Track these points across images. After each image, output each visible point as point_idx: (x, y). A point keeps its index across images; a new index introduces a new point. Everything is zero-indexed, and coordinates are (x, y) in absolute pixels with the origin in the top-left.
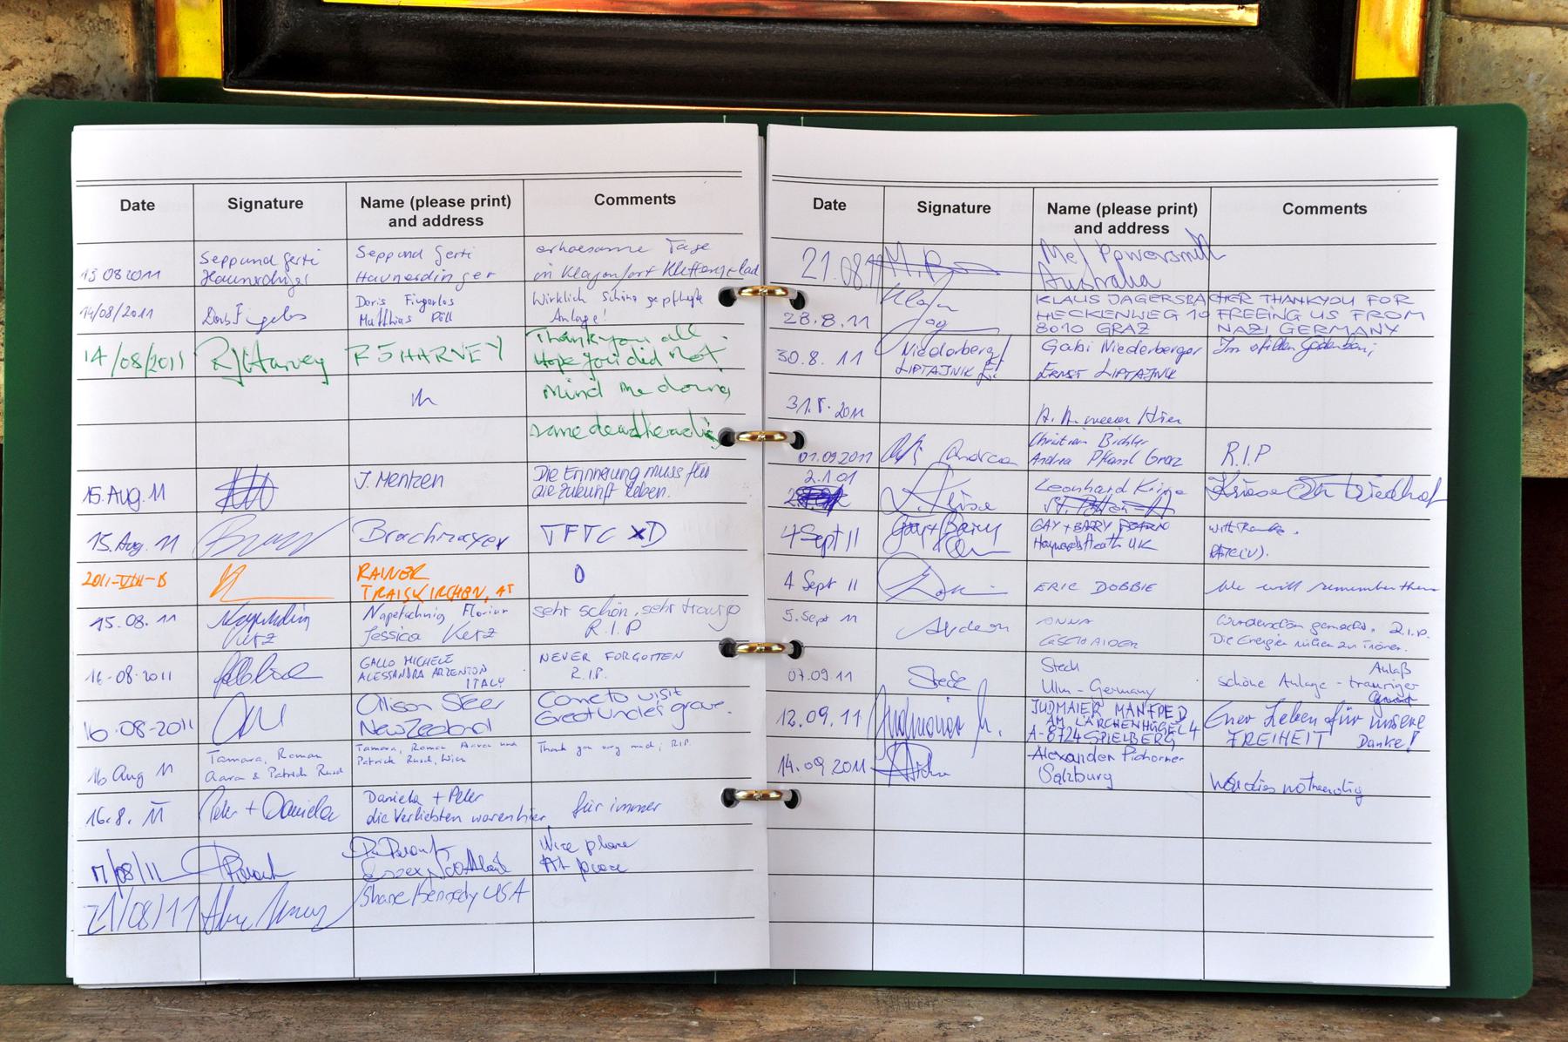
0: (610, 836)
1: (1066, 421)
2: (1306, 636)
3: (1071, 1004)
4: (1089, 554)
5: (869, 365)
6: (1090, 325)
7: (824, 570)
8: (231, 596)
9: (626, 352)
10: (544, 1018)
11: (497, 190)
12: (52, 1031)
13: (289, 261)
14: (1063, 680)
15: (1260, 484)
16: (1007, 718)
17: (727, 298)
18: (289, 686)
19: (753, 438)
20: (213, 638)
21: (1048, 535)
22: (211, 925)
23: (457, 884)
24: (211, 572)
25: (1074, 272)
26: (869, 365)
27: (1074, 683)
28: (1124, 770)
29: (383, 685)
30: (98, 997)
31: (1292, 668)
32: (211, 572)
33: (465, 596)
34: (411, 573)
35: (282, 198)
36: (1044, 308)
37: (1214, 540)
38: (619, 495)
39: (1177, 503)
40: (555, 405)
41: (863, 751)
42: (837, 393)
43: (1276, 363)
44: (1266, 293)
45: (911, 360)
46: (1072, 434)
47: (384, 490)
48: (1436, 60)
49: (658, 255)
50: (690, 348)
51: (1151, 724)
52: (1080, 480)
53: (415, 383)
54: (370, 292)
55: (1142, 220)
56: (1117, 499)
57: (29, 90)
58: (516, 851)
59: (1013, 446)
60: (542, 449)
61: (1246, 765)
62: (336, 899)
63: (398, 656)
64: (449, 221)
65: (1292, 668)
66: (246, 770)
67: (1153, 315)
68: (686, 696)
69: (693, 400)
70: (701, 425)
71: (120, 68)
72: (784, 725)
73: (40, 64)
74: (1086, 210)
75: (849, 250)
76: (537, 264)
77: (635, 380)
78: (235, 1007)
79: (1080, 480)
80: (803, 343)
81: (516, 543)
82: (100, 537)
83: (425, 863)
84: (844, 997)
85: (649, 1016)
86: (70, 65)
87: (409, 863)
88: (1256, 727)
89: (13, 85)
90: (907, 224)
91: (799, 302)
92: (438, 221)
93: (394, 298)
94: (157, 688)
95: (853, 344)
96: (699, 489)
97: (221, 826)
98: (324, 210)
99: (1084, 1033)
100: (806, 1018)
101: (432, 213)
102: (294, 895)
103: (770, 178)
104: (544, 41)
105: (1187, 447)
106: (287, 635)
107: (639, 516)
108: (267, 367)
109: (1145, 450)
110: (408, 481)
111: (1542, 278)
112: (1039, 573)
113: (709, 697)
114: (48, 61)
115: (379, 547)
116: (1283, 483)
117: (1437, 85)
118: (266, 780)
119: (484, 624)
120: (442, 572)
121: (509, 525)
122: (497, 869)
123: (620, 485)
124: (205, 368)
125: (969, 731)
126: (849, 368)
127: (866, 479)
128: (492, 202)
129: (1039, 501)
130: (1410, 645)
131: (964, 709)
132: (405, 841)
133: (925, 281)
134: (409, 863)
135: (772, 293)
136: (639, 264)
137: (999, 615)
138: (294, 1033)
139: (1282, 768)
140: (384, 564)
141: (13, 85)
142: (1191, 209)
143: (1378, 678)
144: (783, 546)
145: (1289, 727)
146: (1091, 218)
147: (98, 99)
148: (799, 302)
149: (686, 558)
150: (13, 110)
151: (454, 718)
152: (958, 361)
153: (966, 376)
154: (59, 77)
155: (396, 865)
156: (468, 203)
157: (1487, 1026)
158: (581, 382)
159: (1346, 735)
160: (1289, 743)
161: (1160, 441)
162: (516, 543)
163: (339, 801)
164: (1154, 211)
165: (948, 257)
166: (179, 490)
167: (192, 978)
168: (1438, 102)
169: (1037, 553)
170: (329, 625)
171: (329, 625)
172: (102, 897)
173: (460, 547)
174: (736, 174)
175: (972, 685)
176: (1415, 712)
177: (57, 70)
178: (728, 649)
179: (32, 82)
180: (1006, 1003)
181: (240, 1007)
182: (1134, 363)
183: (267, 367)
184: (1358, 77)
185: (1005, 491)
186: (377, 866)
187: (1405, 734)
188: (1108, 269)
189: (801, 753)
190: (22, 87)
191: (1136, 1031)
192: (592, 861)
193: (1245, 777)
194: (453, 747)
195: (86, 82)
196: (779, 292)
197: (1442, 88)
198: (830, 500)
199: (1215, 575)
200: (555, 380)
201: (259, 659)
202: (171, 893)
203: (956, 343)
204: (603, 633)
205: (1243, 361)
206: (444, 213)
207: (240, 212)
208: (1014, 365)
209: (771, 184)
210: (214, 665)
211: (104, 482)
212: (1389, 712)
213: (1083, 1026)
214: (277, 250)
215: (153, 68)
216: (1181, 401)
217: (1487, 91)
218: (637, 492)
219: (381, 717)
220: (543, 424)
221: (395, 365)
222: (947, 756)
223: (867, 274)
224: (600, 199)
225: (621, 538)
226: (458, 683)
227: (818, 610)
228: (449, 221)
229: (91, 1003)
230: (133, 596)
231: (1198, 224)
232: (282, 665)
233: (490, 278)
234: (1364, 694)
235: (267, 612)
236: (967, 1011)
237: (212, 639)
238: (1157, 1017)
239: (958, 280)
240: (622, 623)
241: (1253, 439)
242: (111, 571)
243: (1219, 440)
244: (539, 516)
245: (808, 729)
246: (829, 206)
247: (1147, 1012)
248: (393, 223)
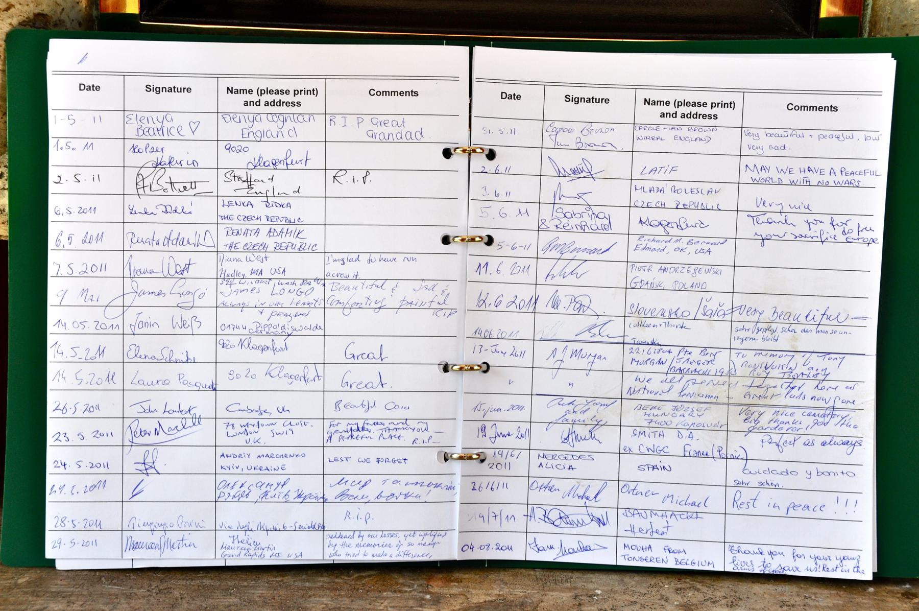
3: (653, 581)
10: (337, 593)
12: (39, 603)
19: (463, 240)
30: (68, 577)
35: (178, 86)
48: (870, 6)
55: (701, 110)
57: (20, 24)
71: (77, 9)
73: (26, 8)
74: (668, 103)
78: (150, 586)
84: (516, 576)
85: (400, 592)
86: (45, 8)
89: (9, 21)
90: (559, 109)
91: (491, 155)
92: (274, 103)
98: (204, 95)
99: (663, 602)
100: (496, 592)
103: (474, 80)
114: (31, 5)
117: (870, 22)
128: (307, 92)
135: (474, 151)
138: (186, 605)
141: (9, 21)
146: (671, 109)
147: (63, 29)
148: (491, 155)
150: (11, 37)
154: (38, 16)
156: (292, 93)
157: (903, 595)
164: (709, 106)
168: (870, 33)
174: (455, 79)
177: (37, 11)
179: (21, 19)
180: (615, 578)
181: (154, 585)
190: (15, 22)
191: (694, 601)
195: (55, 18)
196: (479, 150)
197: (874, 24)
207: (152, 94)
209: (474, 84)
213: (662, 597)
215: (97, 9)
217: (904, 26)
224: (372, 92)
229: (64, 583)
236: (591, 586)
238: (705, 589)
246: (510, 97)
247: (699, 586)
248: (246, 104)
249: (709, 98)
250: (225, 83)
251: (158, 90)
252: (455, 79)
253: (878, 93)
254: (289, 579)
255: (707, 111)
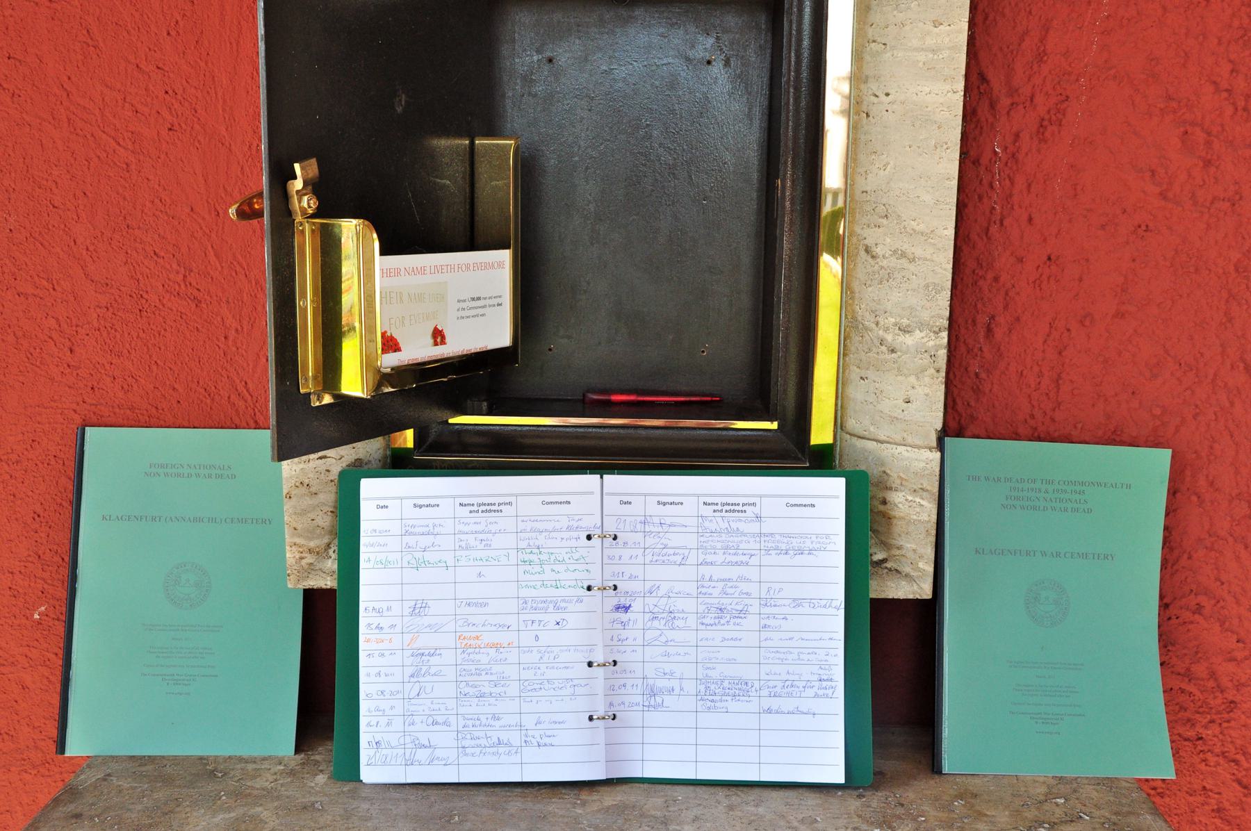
0: (548, 733)
1: (710, 580)
2: (796, 656)
3: (712, 790)
4: (719, 627)
5: (640, 560)
6: (719, 545)
7: (624, 634)
8: (415, 646)
9: (553, 558)
11: (507, 500)
13: (434, 526)
14: (710, 673)
15: (780, 602)
16: (690, 687)
17: (589, 537)
18: (435, 678)
20: (408, 661)
21: (705, 621)
22: (409, 763)
23: (494, 750)
24: (407, 637)
25: (713, 526)
26: (640, 560)
27: (714, 674)
28: (732, 705)
29: (467, 678)
31: (791, 669)
32: (407, 637)
33: (497, 647)
34: (477, 638)
36: (702, 539)
37: (763, 622)
38: (551, 609)
39: (751, 610)
40: (528, 577)
41: (639, 699)
42: (629, 570)
43: (784, 559)
44: (781, 534)
45: (655, 558)
46: (713, 584)
47: (468, 608)
49: (564, 522)
50: (576, 556)
51: (741, 688)
52: (716, 601)
53: (478, 570)
54: (463, 537)
55: (736, 508)
56: (729, 608)
58: (515, 738)
59: (692, 588)
60: (524, 593)
61: (775, 703)
62: (452, 754)
63: (473, 667)
64: (490, 511)
65: (791, 669)
66: (421, 708)
67: (741, 542)
68: (576, 682)
69: (577, 575)
70: (580, 584)
72: (611, 690)
75: (633, 519)
76: (521, 526)
77: (554, 567)
79: (716, 601)
80: (616, 552)
81: (514, 627)
82: (369, 625)
83: (483, 742)
86: (361, 456)
87: (478, 742)
88: (778, 689)
92: (487, 511)
93: (471, 539)
94: (389, 679)
95: (634, 552)
96: (580, 607)
97: (412, 728)
98: (447, 507)
101: (484, 508)
102: (438, 753)
104: (538, 436)
105: (753, 588)
106: (434, 660)
107: (558, 617)
108: (427, 564)
109: (739, 590)
110: (476, 605)
111: (875, 527)
112: (701, 635)
113: (583, 682)
115: (466, 629)
116: (787, 602)
118: (427, 712)
119: (500, 656)
120: (487, 638)
121: (512, 620)
122: (509, 744)
123: (551, 606)
124: (405, 564)
125: (677, 691)
126: (633, 561)
127: (640, 600)
129: (701, 608)
130: (832, 660)
131: (675, 684)
132: (476, 734)
133: (660, 529)
134: (478, 742)
136: (558, 526)
137: (687, 650)
139: (787, 704)
140: (468, 635)
142: (754, 504)
143: (821, 672)
144: (610, 626)
145: (790, 689)
146: (719, 507)
148: (615, 538)
149: (575, 632)
151: (493, 690)
152: (672, 558)
153: (675, 564)
155: (473, 743)
158: (537, 568)
159: (810, 692)
160: (790, 695)
161: (744, 587)
162: (514, 627)
163: (453, 719)
165: (668, 521)
166: (396, 607)
167: (403, 781)
169: (700, 627)
170: (448, 657)
171: (448, 657)
172: (372, 752)
173: (494, 628)
174: (592, 493)
175: (678, 675)
176: (833, 684)
178: (590, 664)
182: (734, 559)
183: (427, 564)
184: (812, 443)
185: (689, 605)
186: (467, 743)
187: (830, 692)
188: (724, 525)
189: (617, 700)
192: (542, 742)
193: (774, 708)
194: (492, 700)
198: (627, 609)
199: (764, 635)
200: (528, 568)
201: (424, 669)
202: (395, 751)
203: (671, 551)
204: (545, 659)
205: (774, 559)
206: (489, 508)
208: (692, 559)
210: (409, 671)
211: (371, 605)
212: (824, 684)
214: (430, 522)
216: (752, 573)
218: (557, 608)
219: (467, 690)
220: (524, 584)
221: (472, 563)
222: (669, 700)
223: (639, 527)
225: (552, 625)
226: (494, 678)
227: (622, 648)
228: (490, 511)
230: (381, 646)
231: (756, 510)
232: (433, 670)
233: (505, 532)
234: (816, 677)
235: (427, 652)
237: (408, 661)
239: (672, 529)
240: (552, 656)
241: (778, 586)
242: (373, 637)
243: (765, 587)
244: (522, 617)
245: (619, 692)
249: (741, 500)
250: (458, 501)
251: (421, 507)
252: (592, 493)
253: (837, 497)
254: (497, 790)
255: (740, 508)
